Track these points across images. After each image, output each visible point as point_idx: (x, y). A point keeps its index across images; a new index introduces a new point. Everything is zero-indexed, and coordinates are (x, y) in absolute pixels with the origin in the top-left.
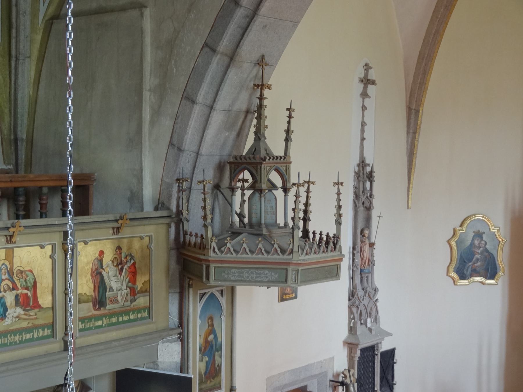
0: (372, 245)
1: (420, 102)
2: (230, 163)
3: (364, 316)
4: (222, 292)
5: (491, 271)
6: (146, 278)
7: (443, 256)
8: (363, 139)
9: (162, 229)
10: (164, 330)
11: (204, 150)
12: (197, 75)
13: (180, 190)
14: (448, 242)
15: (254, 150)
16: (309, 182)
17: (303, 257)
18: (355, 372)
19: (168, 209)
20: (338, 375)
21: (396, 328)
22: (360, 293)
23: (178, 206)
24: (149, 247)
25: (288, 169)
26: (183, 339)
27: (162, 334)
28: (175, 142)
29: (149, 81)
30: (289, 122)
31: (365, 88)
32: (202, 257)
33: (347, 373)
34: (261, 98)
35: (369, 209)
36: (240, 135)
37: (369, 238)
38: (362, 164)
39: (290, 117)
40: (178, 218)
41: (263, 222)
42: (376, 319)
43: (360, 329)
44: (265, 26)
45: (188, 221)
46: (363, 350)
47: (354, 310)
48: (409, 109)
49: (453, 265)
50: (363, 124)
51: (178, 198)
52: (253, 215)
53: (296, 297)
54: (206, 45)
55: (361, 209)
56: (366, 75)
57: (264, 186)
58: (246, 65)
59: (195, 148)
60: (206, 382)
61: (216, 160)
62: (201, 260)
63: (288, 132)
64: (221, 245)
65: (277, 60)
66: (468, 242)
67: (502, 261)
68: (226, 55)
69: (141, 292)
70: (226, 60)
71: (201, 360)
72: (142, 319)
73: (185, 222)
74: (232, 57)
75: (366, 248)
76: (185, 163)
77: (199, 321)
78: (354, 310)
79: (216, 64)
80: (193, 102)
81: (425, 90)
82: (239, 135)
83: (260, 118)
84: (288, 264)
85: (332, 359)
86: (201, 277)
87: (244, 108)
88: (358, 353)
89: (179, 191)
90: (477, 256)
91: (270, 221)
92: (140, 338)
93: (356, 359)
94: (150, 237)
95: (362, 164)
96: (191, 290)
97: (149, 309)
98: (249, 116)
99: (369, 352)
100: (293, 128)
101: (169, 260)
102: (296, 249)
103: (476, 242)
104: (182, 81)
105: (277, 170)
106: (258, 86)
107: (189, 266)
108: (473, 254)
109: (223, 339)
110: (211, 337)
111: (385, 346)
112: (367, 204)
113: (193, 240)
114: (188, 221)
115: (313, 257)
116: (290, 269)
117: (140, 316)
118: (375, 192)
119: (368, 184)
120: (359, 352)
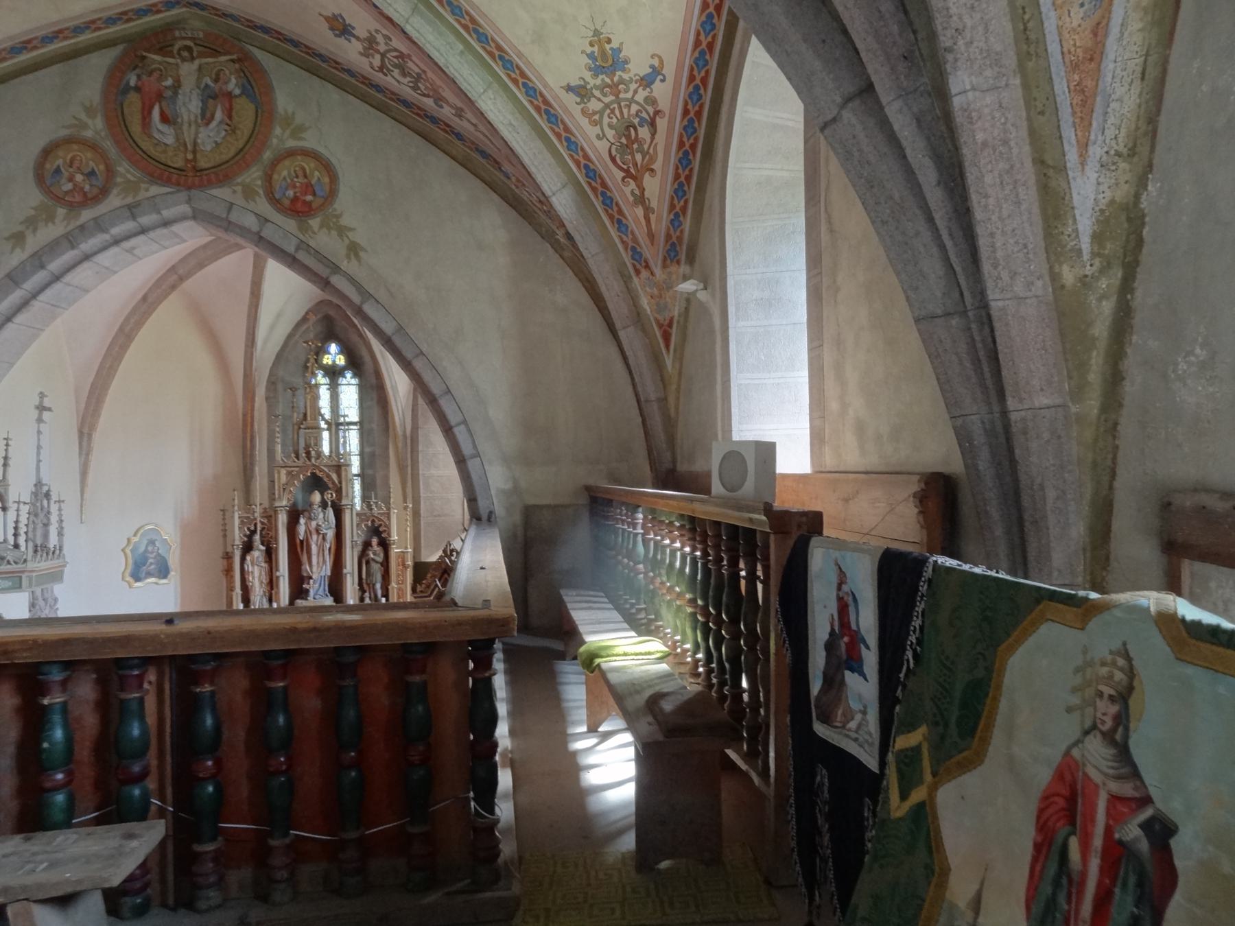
1: (92, 427)
5: (163, 572)
7: (120, 564)
14: (123, 550)
16: (59, 501)
38: (39, 484)
39: (7, 445)
48: (81, 434)
49: (129, 571)
56: (41, 402)
63: (6, 458)
66: (142, 549)
67: (174, 561)
84: (23, 572)
100: (10, 455)
103: (150, 548)
108: (146, 559)
112: (45, 521)
115: (43, 565)
116: (24, 576)
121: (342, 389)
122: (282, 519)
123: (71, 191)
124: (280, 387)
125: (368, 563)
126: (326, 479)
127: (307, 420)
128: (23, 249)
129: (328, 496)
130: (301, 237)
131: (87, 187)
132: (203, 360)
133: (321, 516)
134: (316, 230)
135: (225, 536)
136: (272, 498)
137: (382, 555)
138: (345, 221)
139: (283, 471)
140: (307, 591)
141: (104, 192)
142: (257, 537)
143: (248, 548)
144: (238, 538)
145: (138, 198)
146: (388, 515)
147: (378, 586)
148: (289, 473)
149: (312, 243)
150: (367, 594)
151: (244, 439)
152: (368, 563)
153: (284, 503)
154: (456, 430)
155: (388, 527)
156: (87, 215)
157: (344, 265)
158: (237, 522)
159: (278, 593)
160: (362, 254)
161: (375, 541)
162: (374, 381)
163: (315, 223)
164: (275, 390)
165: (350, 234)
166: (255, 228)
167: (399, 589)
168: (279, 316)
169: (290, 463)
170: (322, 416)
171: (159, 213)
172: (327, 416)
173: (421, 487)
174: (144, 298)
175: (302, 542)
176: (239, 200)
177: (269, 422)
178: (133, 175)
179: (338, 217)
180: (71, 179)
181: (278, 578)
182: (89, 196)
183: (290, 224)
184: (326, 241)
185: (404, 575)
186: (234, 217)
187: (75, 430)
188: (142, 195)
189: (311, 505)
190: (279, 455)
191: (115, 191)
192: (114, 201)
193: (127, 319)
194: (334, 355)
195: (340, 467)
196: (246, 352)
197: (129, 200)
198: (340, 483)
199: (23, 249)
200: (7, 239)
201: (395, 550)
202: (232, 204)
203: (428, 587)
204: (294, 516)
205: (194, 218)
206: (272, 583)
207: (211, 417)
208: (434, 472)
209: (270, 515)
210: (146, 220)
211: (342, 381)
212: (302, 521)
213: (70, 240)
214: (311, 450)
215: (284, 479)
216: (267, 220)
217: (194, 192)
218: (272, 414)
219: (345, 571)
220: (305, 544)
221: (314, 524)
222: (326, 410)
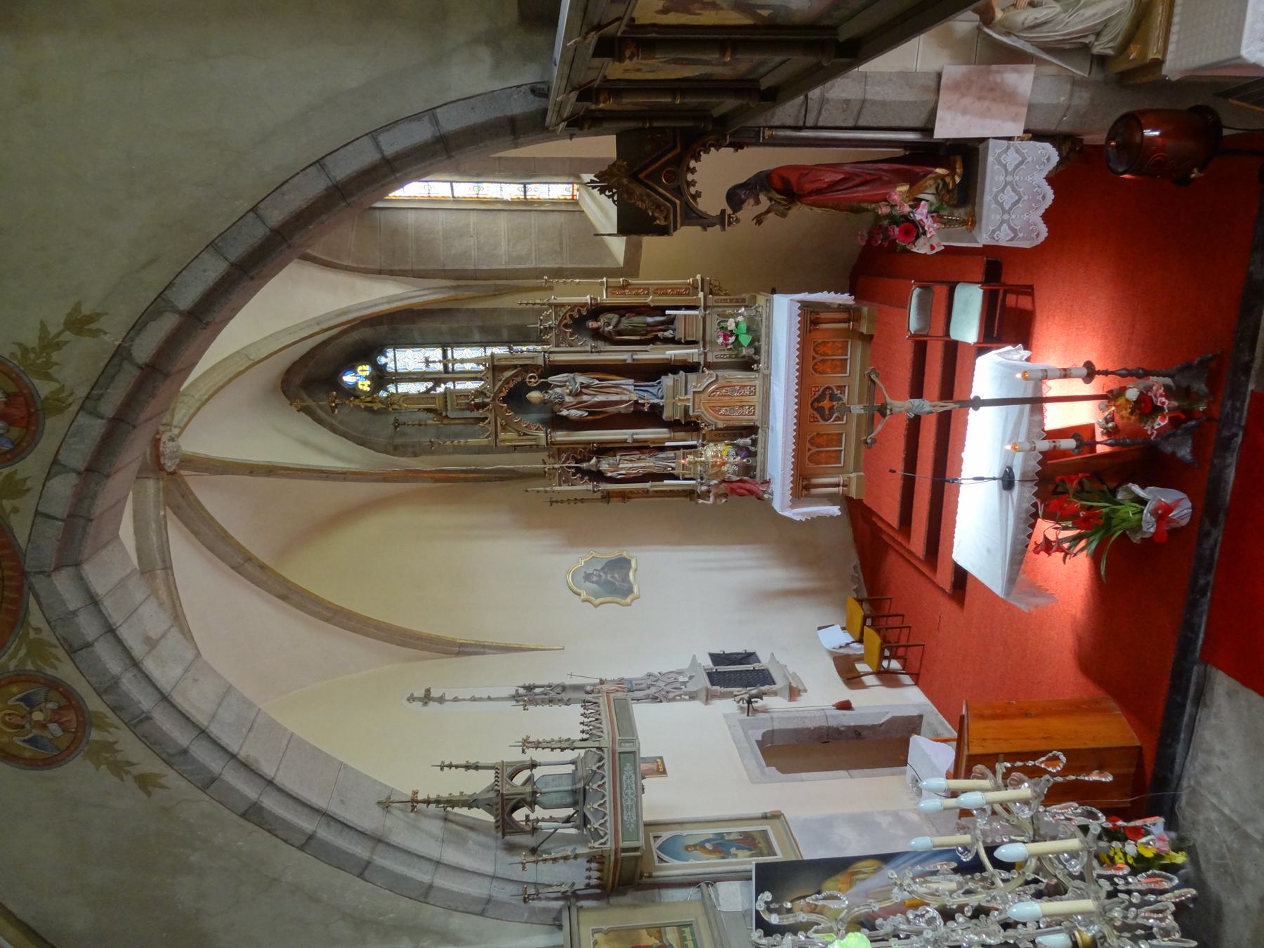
0: (602, 682)
1: (452, 643)
2: (504, 835)
3: (678, 685)
4: (656, 837)
5: (622, 564)
6: (644, 932)
7: (611, 611)
8: (489, 699)
9: (585, 916)
10: (704, 904)
11: (488, 868)
12: (398, 885)
13: (537, 897)
14: (596, 606)
15: (489, 806)
17: (605, 736)
18: (735, 690)
19: (560, 911)
20: (741, 708)
21: (689, 652)
22: (653, 690)
23: (556, 899)
24: (606, 933)
25: (510, 764)
26: (713, 880)
27: (709, 907)
28: (479, 908)
30: (457, 767)
31: (434, 700)
32: (613, 858)
33: (738, 698)
34: (428, 802)
35: (564, 688)
36: (472, 826)
37: (594, 685)
38: (516, 697)
39: (450, 766)
40: (572, 897)
41: (569, 788)
42: (680, 673)
43: (691, 688)
44: (342, 802)
45: (573, 884)
46: (713, 684)
47: (671, 695)
48: (458, 654)
49: (619, 600)
50: (473, 699)
51: (548, 899)
52: (564, 801)
53: (661, 758)
54: (361, 875)
55: (565, 696)
56: (419, 699)
57: (528, 789)
58: (388, 823)
59: (487, 881)
60: (761, 849)
61: (502, 855)
62: (616, 860)
63: (467, 767)
64: (596, 835)
65: (386, 786)
66: (595, 586)
67: (612, 553)
68: (374, 848)
69: (660, 938)
70: (381, 847)
71: (736, 856)
72: (693, 934)
73: (576, 887)
74: (377, 840)
75: (605, 687)
76: (504, 893)
77: (691, 862)
78: (671, 695)
79: (385, 860)
80: (431, 887)
81: (437, 637)
82: (472, 828)
83: (452, 802)
84: (613, 752)
85: (725, 716)
86: (636, 858)
87: (440, 823)
88: (717, 688)
89: (539, 899)
90: (609, 577)
91: (569, 781)
92: (716, 934)
93: (723, 690)
94: (595, 932)
95: (516, 697)
96: (655, 874)
97: (680, 926)
98: (451, 817)
99: (714, 678)
100: (463, 762)
101: (621, 906)
102: (597, 744)
103: (595, 579)
104: (405, 904)
105: (512, 777)
106: (414, 807)
107: (624, 878)
109: (710, 832)
110: (708, 846)
111: (708, 663)
112: (559, 690)
113: (595, 874)
114: (573, 884)
116: (619, 749)
117: (689, 937)
118: (546, 683)
119: (537, 690)
120: (715, 688)
121: (401, 369)
122: (561, 436)
123: (61, 724)
124: (399, 441)
125: (620, 333)
126: (511, 385)
127: (437, 410)
129: (533, 383)
130: (74, 408)
131: (50, 705)
132: (372, 527)
133: (558, 390)
134: (53, 386)
135: (582, 500)
136: (535, 448)
137: (610, 315)
138: (31, 338)
139: (502, 435)
140: (653, 406)
141: (54, 685)
142: (584, 465)
143: (598, 476)
144: (584, 487)
145: (55, 642)
146: (558, 306)
147: (650, 320)
148: (504, 429)
149: (82, 392)
150: (660, 334)
151: (466, 480)
152: (620, 333)
153: (542, 434)
154: (389, 150)
155: (574, 306)
156: (94, 703)
157: (113, 339)
158: (565, 488)
159: (653, 441)
160: (86, 310)
161: (592, 324)
162: (384, 329)
163: (44, 389)
164: (404, 446)
165: (53, 330)
166: (73, 479)
167: (655, 293)
168: (305, 443)
169: (491, 428)
170: (428, 391)
171: (74, 613)
172: (430, 385)
173: (522, 266)
175: (590, 413)
176: (27, 504)
177: (443, 451)
178: (17, 650)
179: (25, 350)
180: (43, 726)
181: (635, 441)
182: (64, 702)
183: (54, 426)
184: (74, 368)
185: (638, 287)
186: (59, 508)
187: (457, 659)
188: (47, 635)
189: (544, 402)
190: (482, 441)
191: (50, 671)
192: (65, 671)
194: (358, 378)
195: (495, 367)
196: (334, 479)
197: (61, 653)
198: (515, 366)
200: (149, 794)
201: (604, 298)
202: (37, 513)
203: (658, 206)
205: (77, 565)
206: (642, 448)
207: (436, 518)
208: (503, 248)
209: (557, 450)
210: (88, 627)
211: (391, 367)
212: (565, 413)
213: (138, 723)
214: (475, 403)
215: (510, 435)
216: (55, 462)
217: (29, 565)
218: (430, 450)
219: (629, 361)
220: (593, 408)
221: (567, 399)
222: (420, 387)
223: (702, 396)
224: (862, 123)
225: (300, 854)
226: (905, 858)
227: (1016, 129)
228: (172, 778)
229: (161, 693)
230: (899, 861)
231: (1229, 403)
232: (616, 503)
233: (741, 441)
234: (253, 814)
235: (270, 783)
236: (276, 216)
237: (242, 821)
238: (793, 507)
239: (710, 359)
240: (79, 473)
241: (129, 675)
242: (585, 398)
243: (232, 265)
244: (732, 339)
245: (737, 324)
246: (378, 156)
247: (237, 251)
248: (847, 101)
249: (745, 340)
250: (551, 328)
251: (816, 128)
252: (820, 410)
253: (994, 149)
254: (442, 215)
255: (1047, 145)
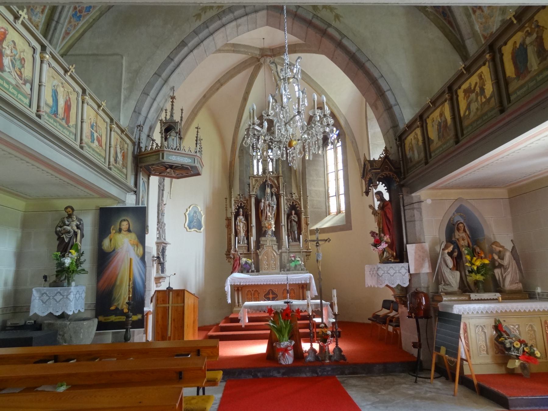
11: (149, 116)
12: (150, 85)
28: (137, 110)
29: (124, 85)
54: (155, 73)
70: (163, 82)
74: (166, 81)
76: (141, 120)
79: (160, 82)
104: (142, 87)
122: (253, 200)
125: (291, 222)
128: (200, 20)
129: (273, 190)
130: (314, 13)
133: (270, 199)
143: (237, 215)
147: (296, 232)
149: (319, 15)
152: (291, 222)
155: (300, 205)
157: (333, 23)
160: (341, 18)
161: (293, 212)
165: (335, 11)
174: (204, 96)
175: (262, 211)
181: (251, 227)
193: (196, 105)
198: (279, 184)
199: (200, 20)
204: (258, 202)
215: (254, 182)
223: (271, 250)
224: (407, 224)
225: (166, 56)
226: (143, 268)
227: (412, 272)
228: (199, 23)
229: (226, 25)
230: (141, 265)
231: (330, 369)
232: (225, 222)
233: (253, 266)
234: (183, 44)
235: (192, 51)
236: (368, 65)
237: (181, 40)
238: (231, 285)
239: (283, 254)
240: (296, 12)
241: (232, 17)
242: (268, 208)
243: (354, 54)
244: (293, 259)
245: (298, 261)
246: (385, 90)
247: (358, 55)
248: (414, 216)
249: (293, 264)
250: (292, 197)
251: (404, 210)
252: (268, 293)
253: (405, 265)
254: (323, 169)
255: (408, 283)
